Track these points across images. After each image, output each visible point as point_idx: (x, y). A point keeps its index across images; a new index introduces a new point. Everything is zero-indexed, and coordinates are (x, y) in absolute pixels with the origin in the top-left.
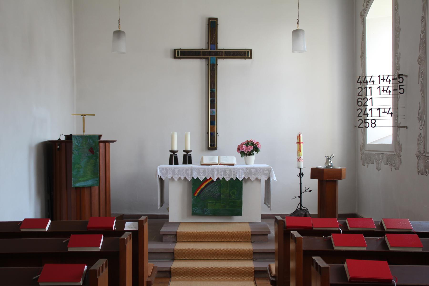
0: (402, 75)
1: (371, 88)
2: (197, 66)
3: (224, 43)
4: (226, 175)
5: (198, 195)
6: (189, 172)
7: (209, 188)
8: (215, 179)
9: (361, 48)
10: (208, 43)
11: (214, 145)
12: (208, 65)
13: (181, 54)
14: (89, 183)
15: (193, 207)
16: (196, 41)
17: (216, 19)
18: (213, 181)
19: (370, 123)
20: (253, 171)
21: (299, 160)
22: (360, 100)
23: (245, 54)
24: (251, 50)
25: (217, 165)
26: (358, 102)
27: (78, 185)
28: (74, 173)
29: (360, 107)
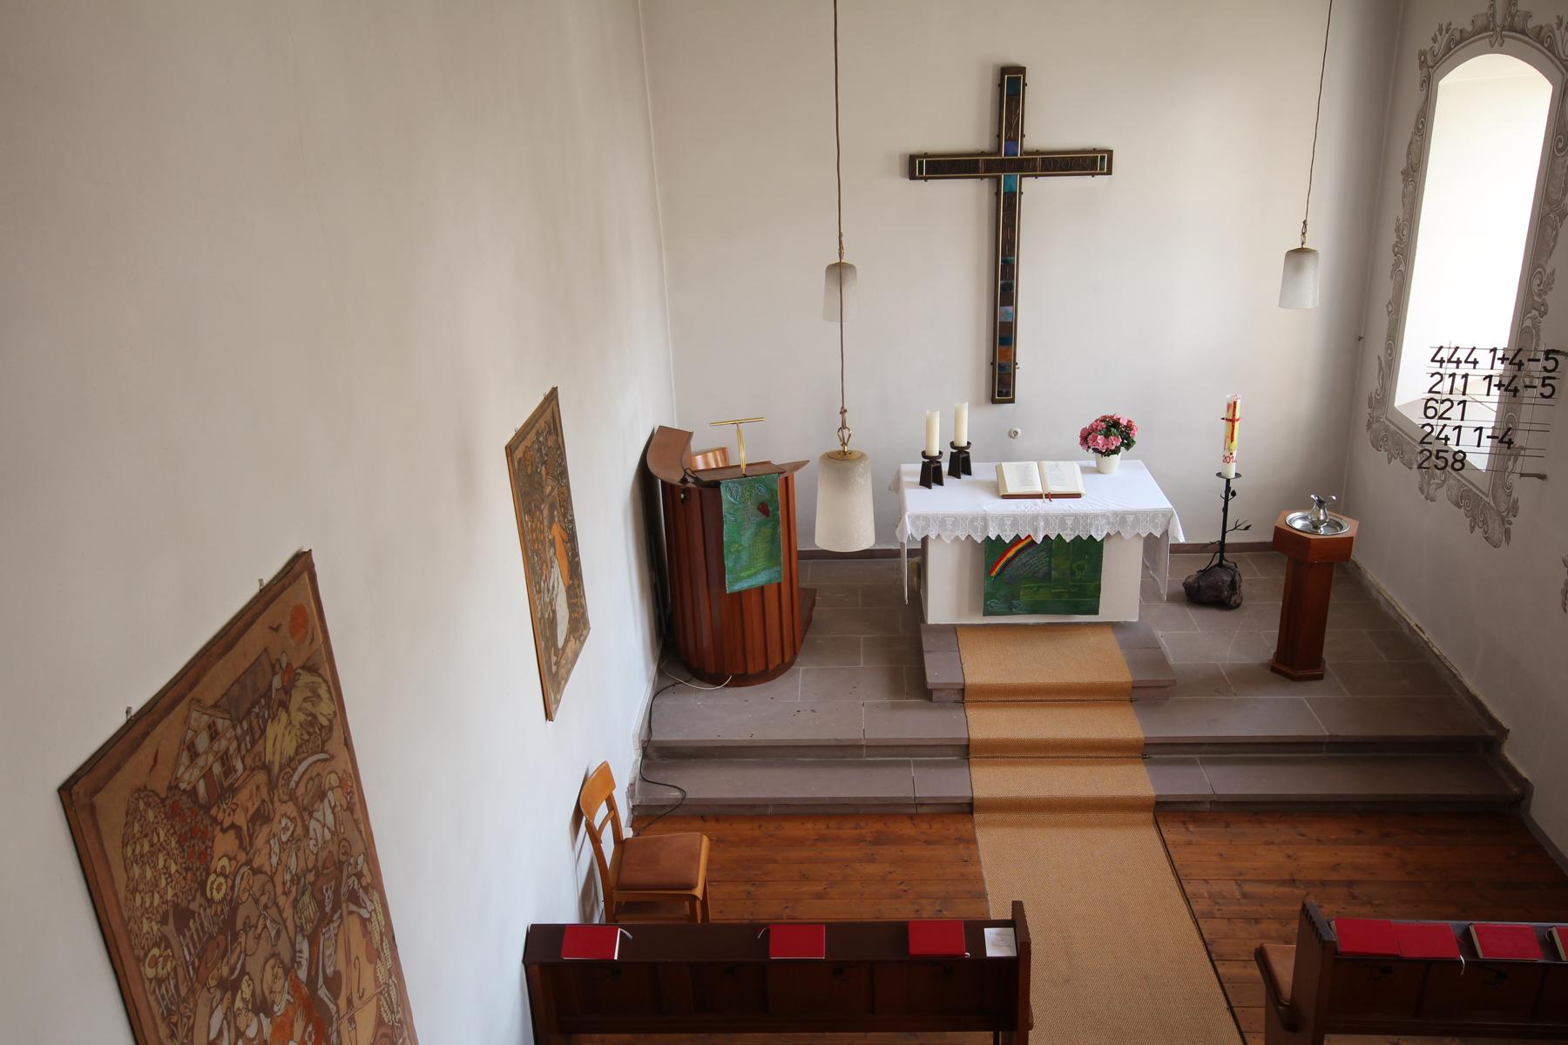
0: (1557, 352)
1: (1466, 376)
2: (966, 198)
3: (1040, 134)
4: (1064, 529)
5: (999, 574)
6: (979, 524)
7: (1023, 558)
8: (1039, 540)
9: (1409, 153)
10: (999, 136)
11: (1007, 394)
12: (998, 194)
13: (930, 166)
14: (761, 579)
15: (986, 600)
16: (966, 131)
17: (1022, 70)
18: (1033, 543)
19: (1451, 461)
20: (1130, 519)
21: (1227, 459)
22: (1431, 403)
23: (1091, 162)
24: (1110, 152)
25: (1039, 496)
26: (1426, 408)
27: (737, 587)
28: (729, 563)
29: (1432, 422)
